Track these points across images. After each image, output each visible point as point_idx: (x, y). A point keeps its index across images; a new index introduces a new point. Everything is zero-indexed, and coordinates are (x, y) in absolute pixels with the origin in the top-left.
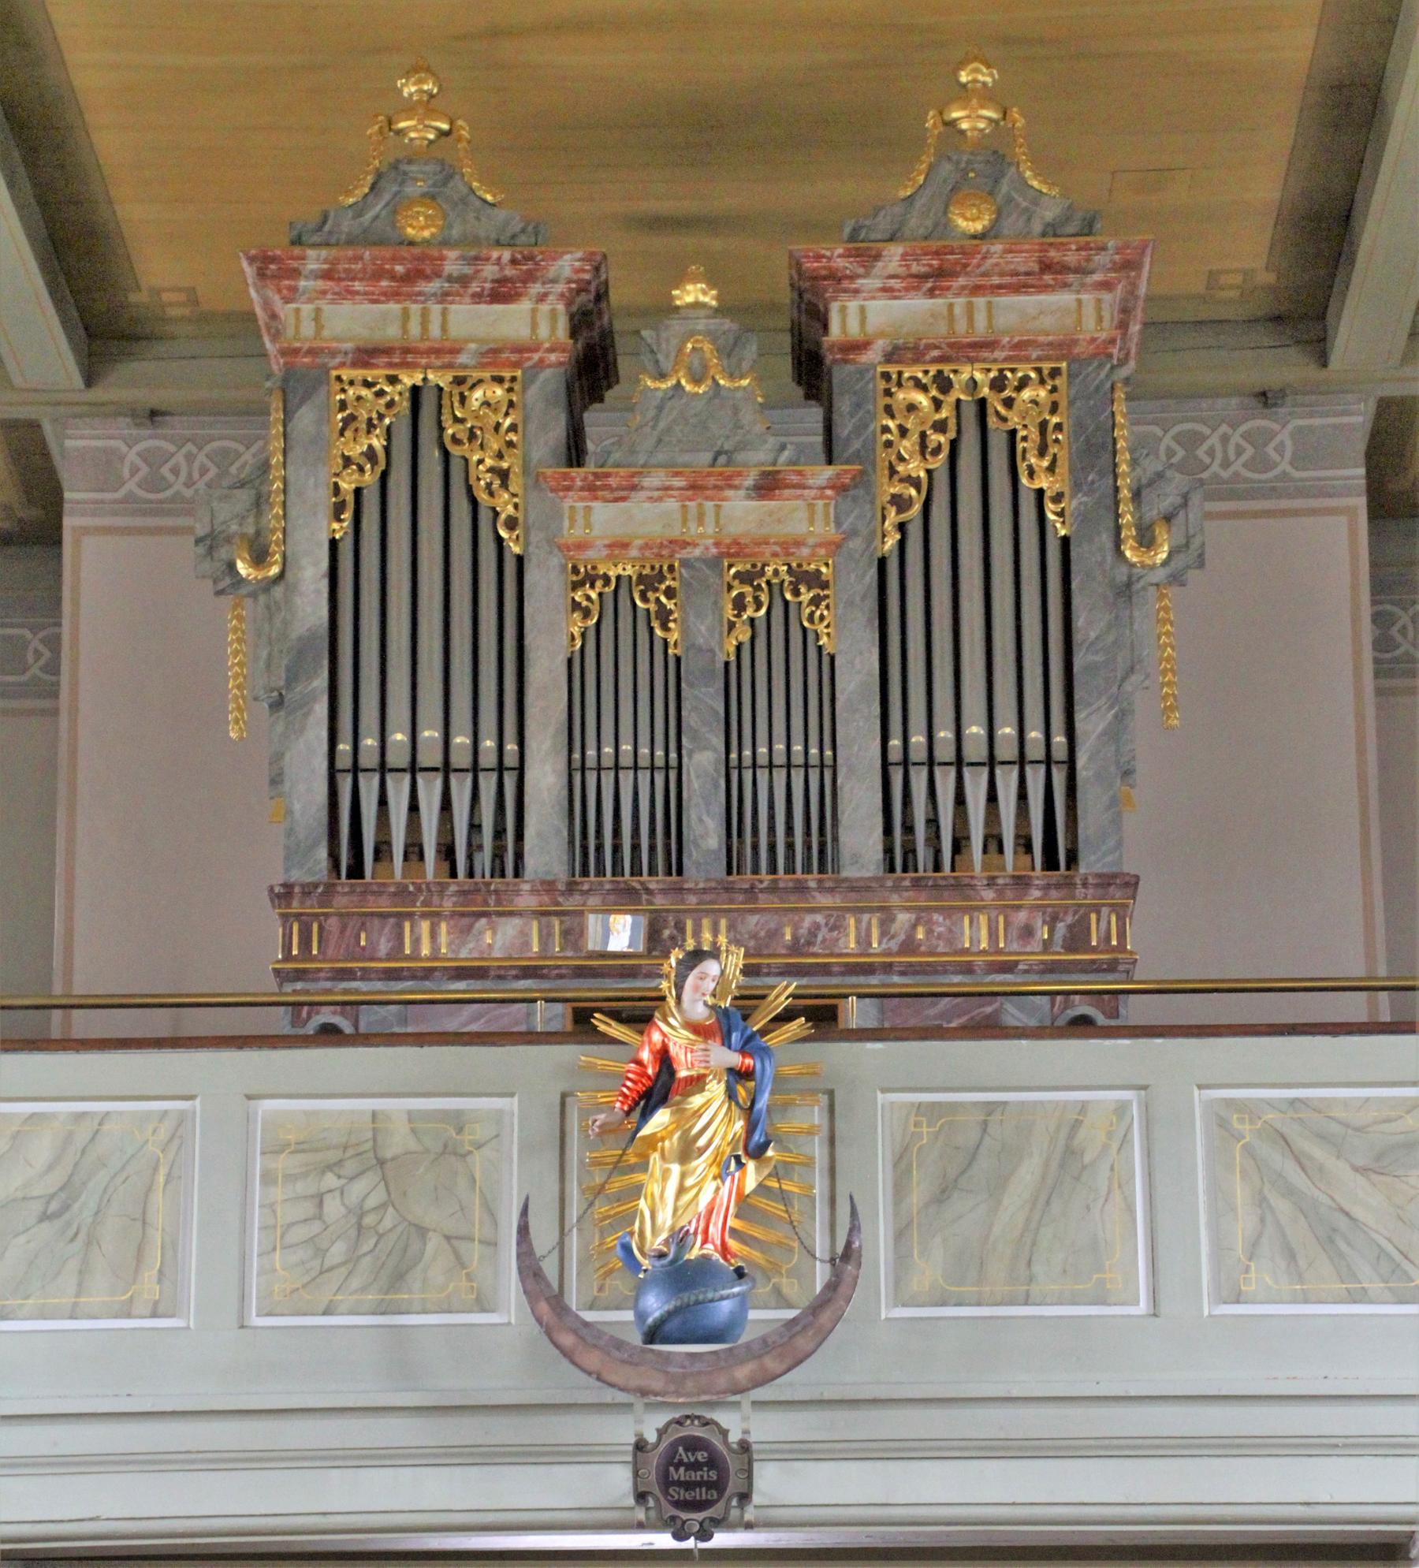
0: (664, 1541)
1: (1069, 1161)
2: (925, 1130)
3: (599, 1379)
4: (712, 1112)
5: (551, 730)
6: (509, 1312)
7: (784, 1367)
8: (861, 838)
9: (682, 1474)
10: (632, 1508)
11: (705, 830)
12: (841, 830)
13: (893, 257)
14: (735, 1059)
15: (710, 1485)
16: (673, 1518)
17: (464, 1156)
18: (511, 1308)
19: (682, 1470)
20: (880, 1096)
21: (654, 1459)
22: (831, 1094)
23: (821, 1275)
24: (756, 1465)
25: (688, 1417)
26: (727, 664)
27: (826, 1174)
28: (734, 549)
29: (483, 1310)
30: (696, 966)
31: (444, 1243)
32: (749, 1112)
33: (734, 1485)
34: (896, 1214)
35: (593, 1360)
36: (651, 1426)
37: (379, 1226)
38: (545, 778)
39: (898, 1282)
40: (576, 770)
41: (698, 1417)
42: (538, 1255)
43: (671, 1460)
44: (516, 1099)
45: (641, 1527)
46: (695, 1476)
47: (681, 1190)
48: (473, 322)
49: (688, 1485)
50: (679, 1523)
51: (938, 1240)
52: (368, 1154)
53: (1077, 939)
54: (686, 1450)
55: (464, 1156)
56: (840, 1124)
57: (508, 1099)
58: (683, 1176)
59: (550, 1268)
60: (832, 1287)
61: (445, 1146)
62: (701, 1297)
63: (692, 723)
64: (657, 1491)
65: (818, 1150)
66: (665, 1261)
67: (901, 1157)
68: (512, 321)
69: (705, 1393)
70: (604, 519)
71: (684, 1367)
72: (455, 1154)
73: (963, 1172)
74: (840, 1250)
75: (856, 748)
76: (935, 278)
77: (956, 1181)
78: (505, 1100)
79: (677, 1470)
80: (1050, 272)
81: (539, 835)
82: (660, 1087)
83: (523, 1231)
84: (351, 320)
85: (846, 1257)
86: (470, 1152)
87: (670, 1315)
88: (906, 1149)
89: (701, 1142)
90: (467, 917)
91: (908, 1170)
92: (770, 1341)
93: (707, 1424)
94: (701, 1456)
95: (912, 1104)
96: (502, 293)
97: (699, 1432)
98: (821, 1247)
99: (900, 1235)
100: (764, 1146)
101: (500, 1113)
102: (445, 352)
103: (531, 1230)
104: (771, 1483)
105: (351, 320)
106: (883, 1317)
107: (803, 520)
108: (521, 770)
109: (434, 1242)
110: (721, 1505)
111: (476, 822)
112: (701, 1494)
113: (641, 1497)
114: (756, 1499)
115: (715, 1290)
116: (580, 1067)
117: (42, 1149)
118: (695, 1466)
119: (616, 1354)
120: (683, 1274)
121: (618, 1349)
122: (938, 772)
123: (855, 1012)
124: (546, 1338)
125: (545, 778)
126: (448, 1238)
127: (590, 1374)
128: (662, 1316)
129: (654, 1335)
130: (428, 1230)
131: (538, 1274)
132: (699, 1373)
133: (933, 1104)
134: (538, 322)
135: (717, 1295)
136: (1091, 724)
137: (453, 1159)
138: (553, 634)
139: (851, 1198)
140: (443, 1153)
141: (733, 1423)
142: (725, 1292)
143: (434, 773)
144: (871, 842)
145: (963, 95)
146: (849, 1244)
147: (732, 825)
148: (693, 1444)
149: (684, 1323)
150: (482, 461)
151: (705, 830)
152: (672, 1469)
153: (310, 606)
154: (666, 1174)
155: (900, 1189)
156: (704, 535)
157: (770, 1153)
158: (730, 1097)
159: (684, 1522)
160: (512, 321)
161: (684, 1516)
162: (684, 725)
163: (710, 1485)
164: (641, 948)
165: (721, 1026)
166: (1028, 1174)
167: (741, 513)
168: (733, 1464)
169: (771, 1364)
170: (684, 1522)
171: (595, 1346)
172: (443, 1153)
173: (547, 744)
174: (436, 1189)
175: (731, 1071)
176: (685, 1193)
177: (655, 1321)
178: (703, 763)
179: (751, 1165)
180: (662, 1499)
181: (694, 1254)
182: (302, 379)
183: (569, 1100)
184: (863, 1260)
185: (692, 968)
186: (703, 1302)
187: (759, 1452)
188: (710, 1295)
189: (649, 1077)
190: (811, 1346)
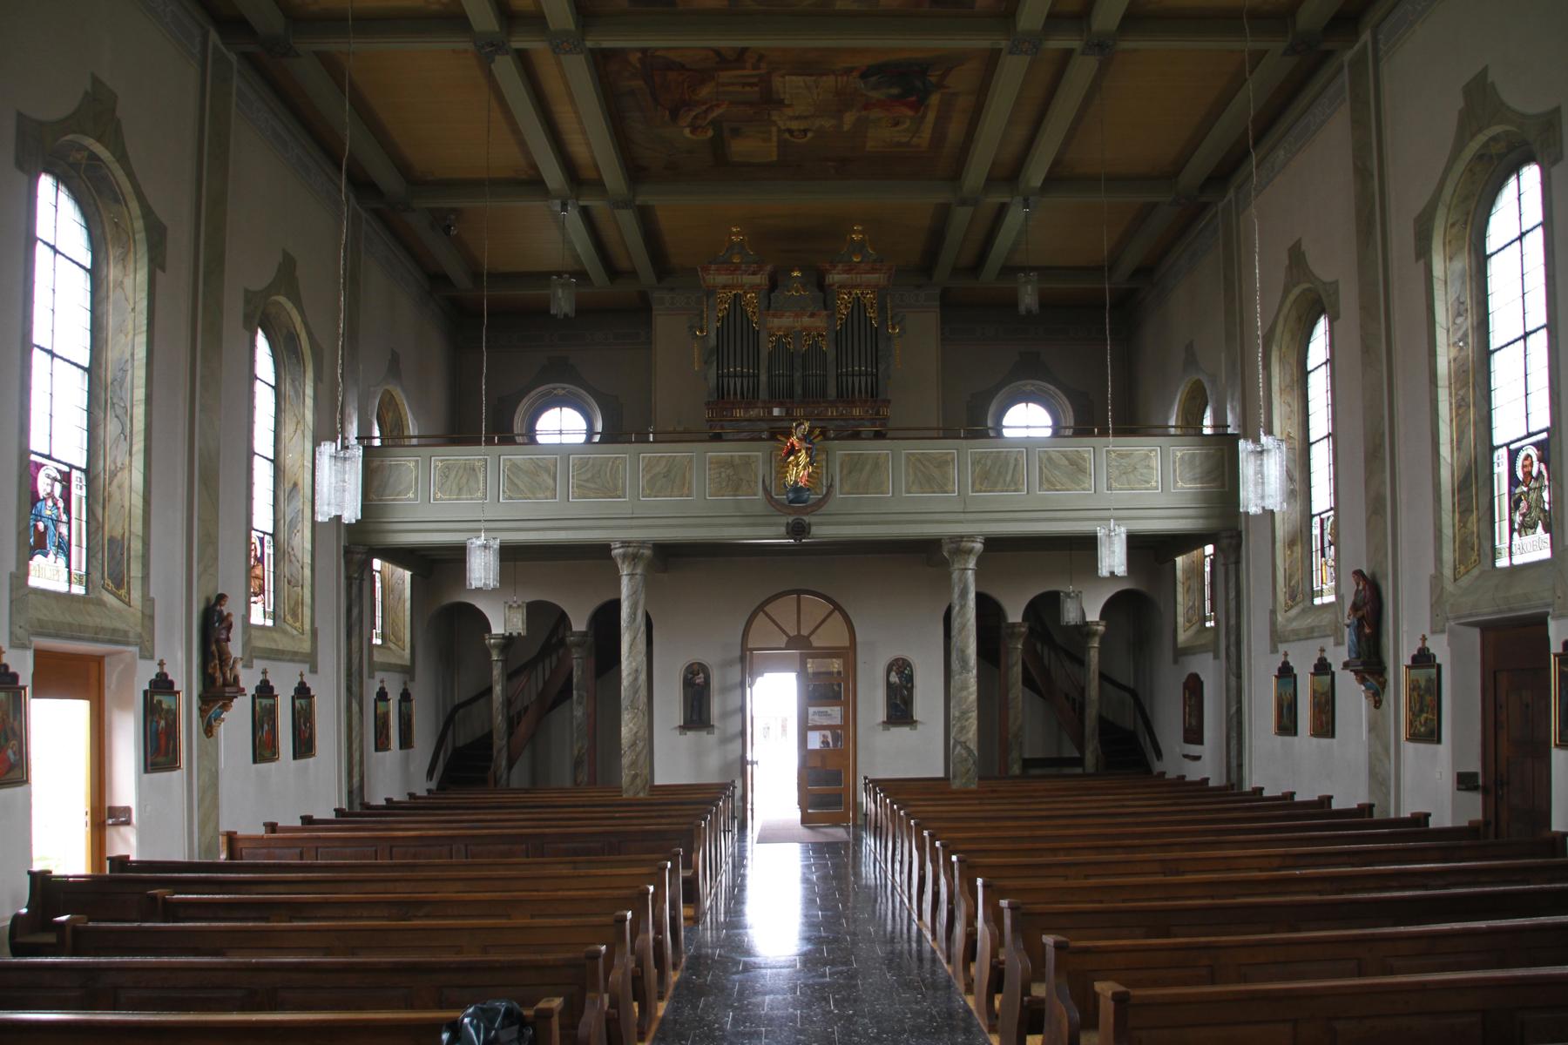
1: (876, 466)
4: (803, 458)
8: (832, 391)
11: (798, 390)
13: (840, 266)
18: (760, 495)
28: (805, 329)
36: (790, 519)
37: (734, 479)
38: (763, 378)
40: (770, 377)
48: (748, 279)
52: (730, 464)
53: (878, 413)
68: (757, 279)
70: (776, 322)
76: (848, 272)
78: (757, 454)
80: (873, 271)
82: (793, 451)
84: (721, 279)
85: (830, 487)
90: (747, 409)
96: (754, 273)
102: (742, 286)
104: (814, 530)
105: (721, 279)
107: (819, 322)
117: (663, 463)
120: (796, 489)
123: (832, 434)
125: (763, 378)
134: (760, 279)
136: (882, 367)
138: (766, 347)
141: (806, 519)
145: (855, 232)
147: (804, 389)
150: (750, 310)
151: (798, 390)
153: (713, 341)
156: (798, 325)
160: (757, 279)
164: (966, 781)
165: (804, 438)
166: (868, 467)
167: (806, 321)
176: (798, 472)
178: (798, 375)
182: (711, 292)
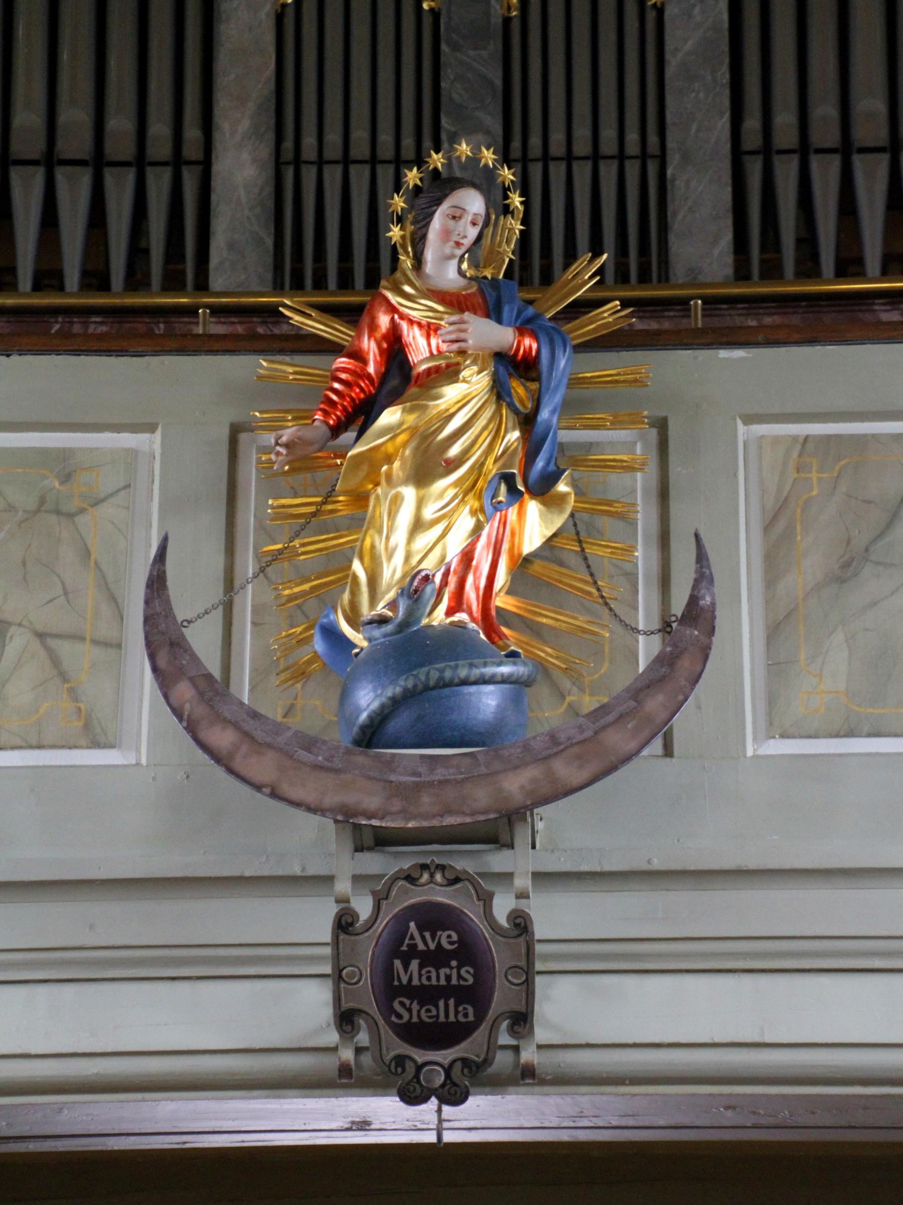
0: (393, 1121)
2: (814, 475)
3: (274, 795)
5: (251, 106)
6: (138, 751)
7: (585, 775)
9: (413, 973)
10: (335, 1049)
12: (672, 238)
14: (503, 336)
15: (463, 995)
16: (400, 1060)
17: (70, 516)
19: (414, 964)
20: (741, 428)
21: (367, 950)
22: (662, 425)
23: (647, 649)
24: (538, 979)
25: (424, 867)
26: (507, 21)
27: (654, 499)
29: (96, 744)
30: (445, 196)
31: (36, 645)
32: (527, 422)
33: (502, 998)
34: (769, 602)
35: (263, 768)
39: (772, 700)
40: (285, 164)
41: (442, 868)
42: (180, 619)
43: (397, 949)
44: (158, 434)
45: (346, 1080)
46: (438, 977)
47: (418, 525)
49: (426, 995)
50: (410, 1069)
51: (839, 637)
54: (421, 929)
55: (70, 516)
56: (676, 469)
57: (146, 436)
58: (420, 504)
59: (203, 640)
60: (665, 662)
61: (42, 501)
62: (448, 674)
63: (455, 96)
64: (373, 1009)
65: (641, 484)
66: (389, 628)
67: (775, 517)
69: (450, 812)
71: (415, 774)
72: (58, 512)
73: (881, 535)
74: (678, 606)
75: (694, 127)
77: (867, 550)
79: (406, 966)
81: (231, 246)
83: (157, 583)
85: (691, 629)
86: (82, 511)
87: (394, 706)
88: (783, 505)
89: (454, 451)
91: (788, 535)
92: (563, 737)
93: (457, 880)
94: (447, 939)
95: (795, 438)
97: (442, 896)
98: (645, 615)
99: (775, 631)
100: (550, 479)
101: (133, 454)
103: (170, 583)
104: (566, 1009)
106: (750, 753)
108: (206, 164)
109: (18, 642)
110: (480, 1034)
111: (143, 245)
112: (447, 1011)
113: (346, 1019)
114: (541, 1035)
115: (472, 666)
116: (260, 377)
118: (435, 958)
119: (303, 754)
121: (308, 750)
122: (815, 162)
124: (188, 738)
126: (41, 636)
127: (258, 788)
128: (383, 706)
129: (371, 735)
130: (9, 624)
131: (178, 645)
132: (443, 783)
133: (829, 438)
135: (476, 672)
137: (53, 519)
139: (697, 536)
140: (38, 511)
142: (489, 670)
143: (77, 169)
144: (716, 252)
146: (693, 600)
148: (433, 917)
149: (420, 718)
152: (398, 963)
154: (397, 501)
155: (774, 564)
157: (562, 487)
158: (499, 397)
159: (419, 1068)
161: (420, 1056)
162: (444, 100)
163: (463, 995)
168: (501, 956)
169: (566, 771)
170: (419, 1068)
171: (270, 746)
172: (38, 511)
173: (245, 125)
174: (24, 564)
175: (500, 356)
176: (424, 533)
177: (370, 718)
179: (533, 507)
180: (381, 1022)
181: (439, 616)
183: (243, 437)
184: (718, 622)
185: (438, 202)
186: (450, 684)
187: (546, 957)
188: (463, 673)
189: (369, 376)
190: (633, 745)
